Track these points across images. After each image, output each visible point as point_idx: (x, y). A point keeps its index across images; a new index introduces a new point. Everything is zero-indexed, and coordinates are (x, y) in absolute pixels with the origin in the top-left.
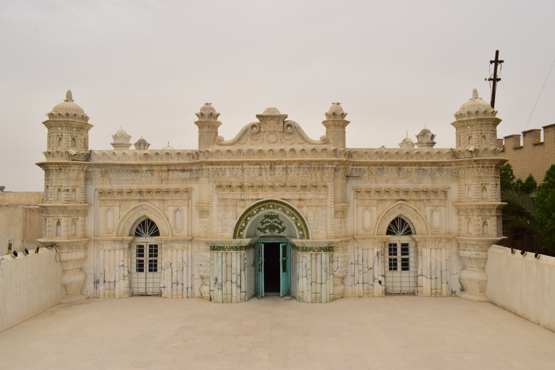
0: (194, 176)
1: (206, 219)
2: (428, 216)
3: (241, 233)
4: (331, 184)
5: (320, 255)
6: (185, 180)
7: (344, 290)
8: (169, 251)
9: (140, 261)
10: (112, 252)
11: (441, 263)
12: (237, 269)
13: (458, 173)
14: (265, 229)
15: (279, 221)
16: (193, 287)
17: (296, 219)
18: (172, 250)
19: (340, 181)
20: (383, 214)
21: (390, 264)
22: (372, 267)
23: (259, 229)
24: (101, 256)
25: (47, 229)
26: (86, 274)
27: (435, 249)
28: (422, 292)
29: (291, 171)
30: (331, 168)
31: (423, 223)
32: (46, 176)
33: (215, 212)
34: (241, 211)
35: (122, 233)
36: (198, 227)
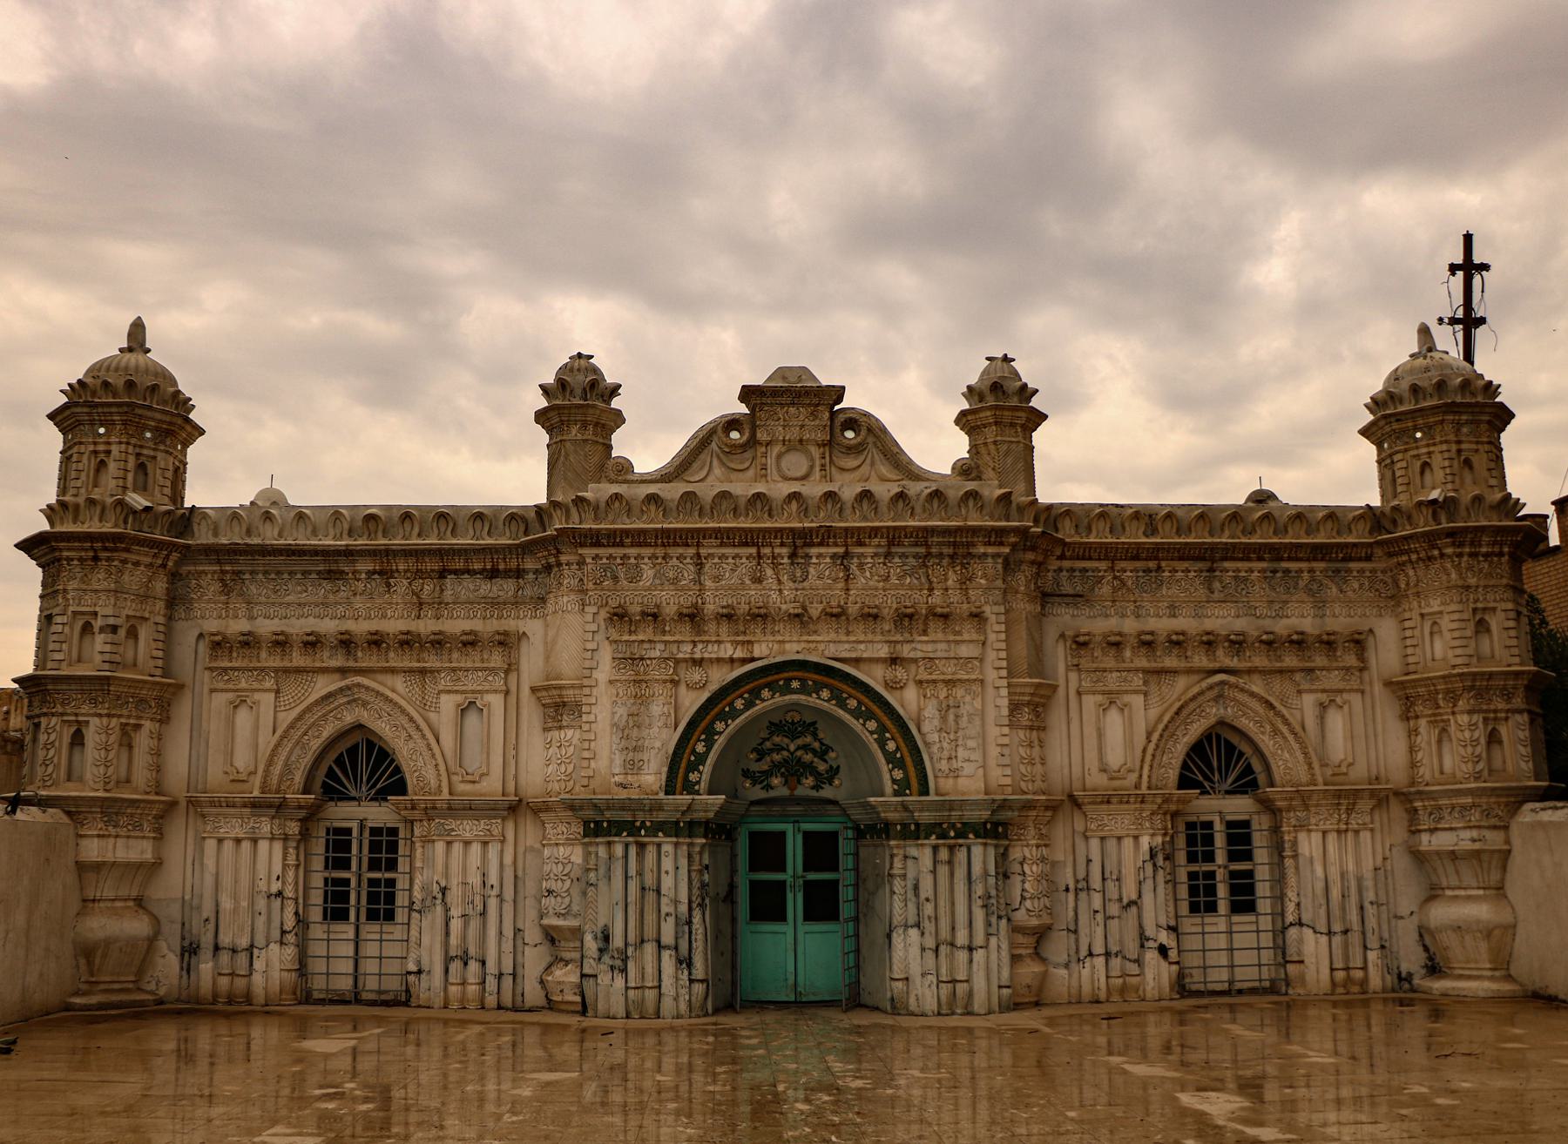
0: (528, 592)
1: (570, 733)
2: (1311, 723)
3: (693, 777)
4: (996, 609)
5: (964, 849)
6: (494, 603)
7: (1044, 976)
8: (440, 847)
9: (336, 882)
10: (246, 845)
11: (1360, 880)
12: (676, 902)
13: (1396, 583)
14: (768, 774)
15: (816, 745)
16: (520, 971)
17: (882, 729)
18: (449, 843)
19: (1024, 607)
20: (1166, 718)
21: (1193, 891)
22: (1134, 897)
23: (746, 774)
24: (210, 862)
25: (41, 754)
26: (158, 921)
27: (1339, 832)
28: (1302, 979)
29: (861, 566)
30: (995, 556)
31: (1296, 746)
32: (44, 585)
33: (605, 708)
34: (691, 702)
35: (280, 782)
36: (542, 764)
